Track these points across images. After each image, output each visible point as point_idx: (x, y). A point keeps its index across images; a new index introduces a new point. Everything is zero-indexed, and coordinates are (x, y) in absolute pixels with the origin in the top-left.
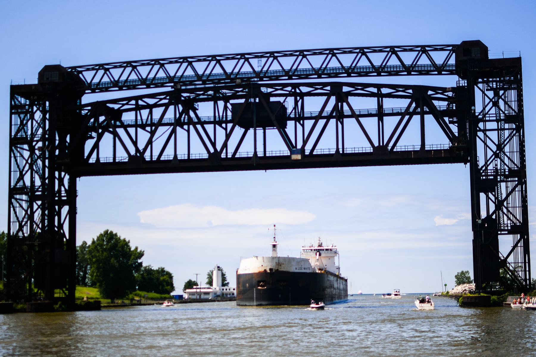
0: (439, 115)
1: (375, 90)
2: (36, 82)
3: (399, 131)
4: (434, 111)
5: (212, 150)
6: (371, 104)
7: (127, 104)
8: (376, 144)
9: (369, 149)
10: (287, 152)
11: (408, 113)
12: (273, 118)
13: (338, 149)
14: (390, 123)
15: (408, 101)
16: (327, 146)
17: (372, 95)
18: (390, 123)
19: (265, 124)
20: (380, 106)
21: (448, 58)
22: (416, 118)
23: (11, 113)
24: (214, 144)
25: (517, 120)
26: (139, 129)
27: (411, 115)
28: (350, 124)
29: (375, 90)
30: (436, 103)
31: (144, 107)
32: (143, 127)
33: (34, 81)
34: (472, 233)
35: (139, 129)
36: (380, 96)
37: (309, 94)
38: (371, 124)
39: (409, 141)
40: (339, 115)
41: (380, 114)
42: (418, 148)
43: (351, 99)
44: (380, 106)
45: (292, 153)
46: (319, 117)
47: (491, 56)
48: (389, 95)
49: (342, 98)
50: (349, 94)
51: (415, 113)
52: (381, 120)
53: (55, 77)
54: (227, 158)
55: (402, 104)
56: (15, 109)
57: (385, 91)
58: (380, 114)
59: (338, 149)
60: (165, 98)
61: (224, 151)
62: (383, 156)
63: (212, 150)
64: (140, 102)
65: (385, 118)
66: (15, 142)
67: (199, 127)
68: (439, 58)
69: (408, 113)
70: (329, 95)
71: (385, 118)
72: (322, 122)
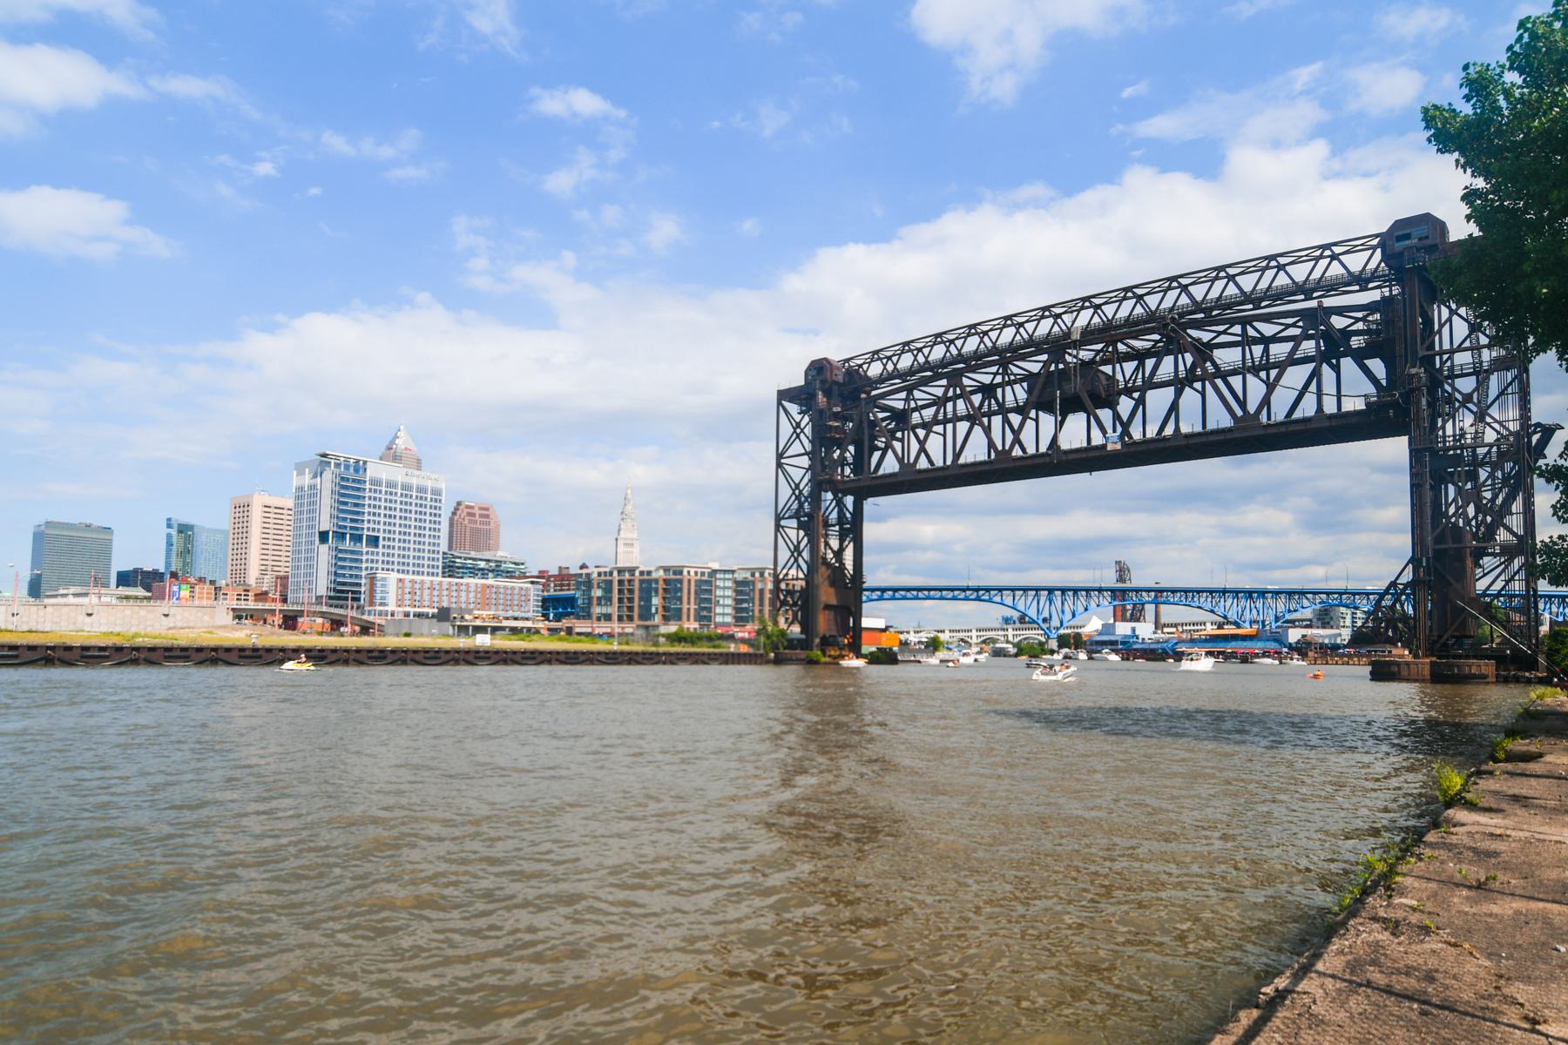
0: (1360, 357)
4: (1350, 352)
5: (1239, 413)
7: (1224, 332)
16: (976, 452)
24: (1243, 404)
26: (1249, 376)
31: (1255, 341)
32: (1255, 370)
35: (1249, 376)
54: (1145, 442)
60: (1294, 325)
61: (1265, 412)
63: (1239, 413)
64: (1121, 347)
67: (1219, 382)
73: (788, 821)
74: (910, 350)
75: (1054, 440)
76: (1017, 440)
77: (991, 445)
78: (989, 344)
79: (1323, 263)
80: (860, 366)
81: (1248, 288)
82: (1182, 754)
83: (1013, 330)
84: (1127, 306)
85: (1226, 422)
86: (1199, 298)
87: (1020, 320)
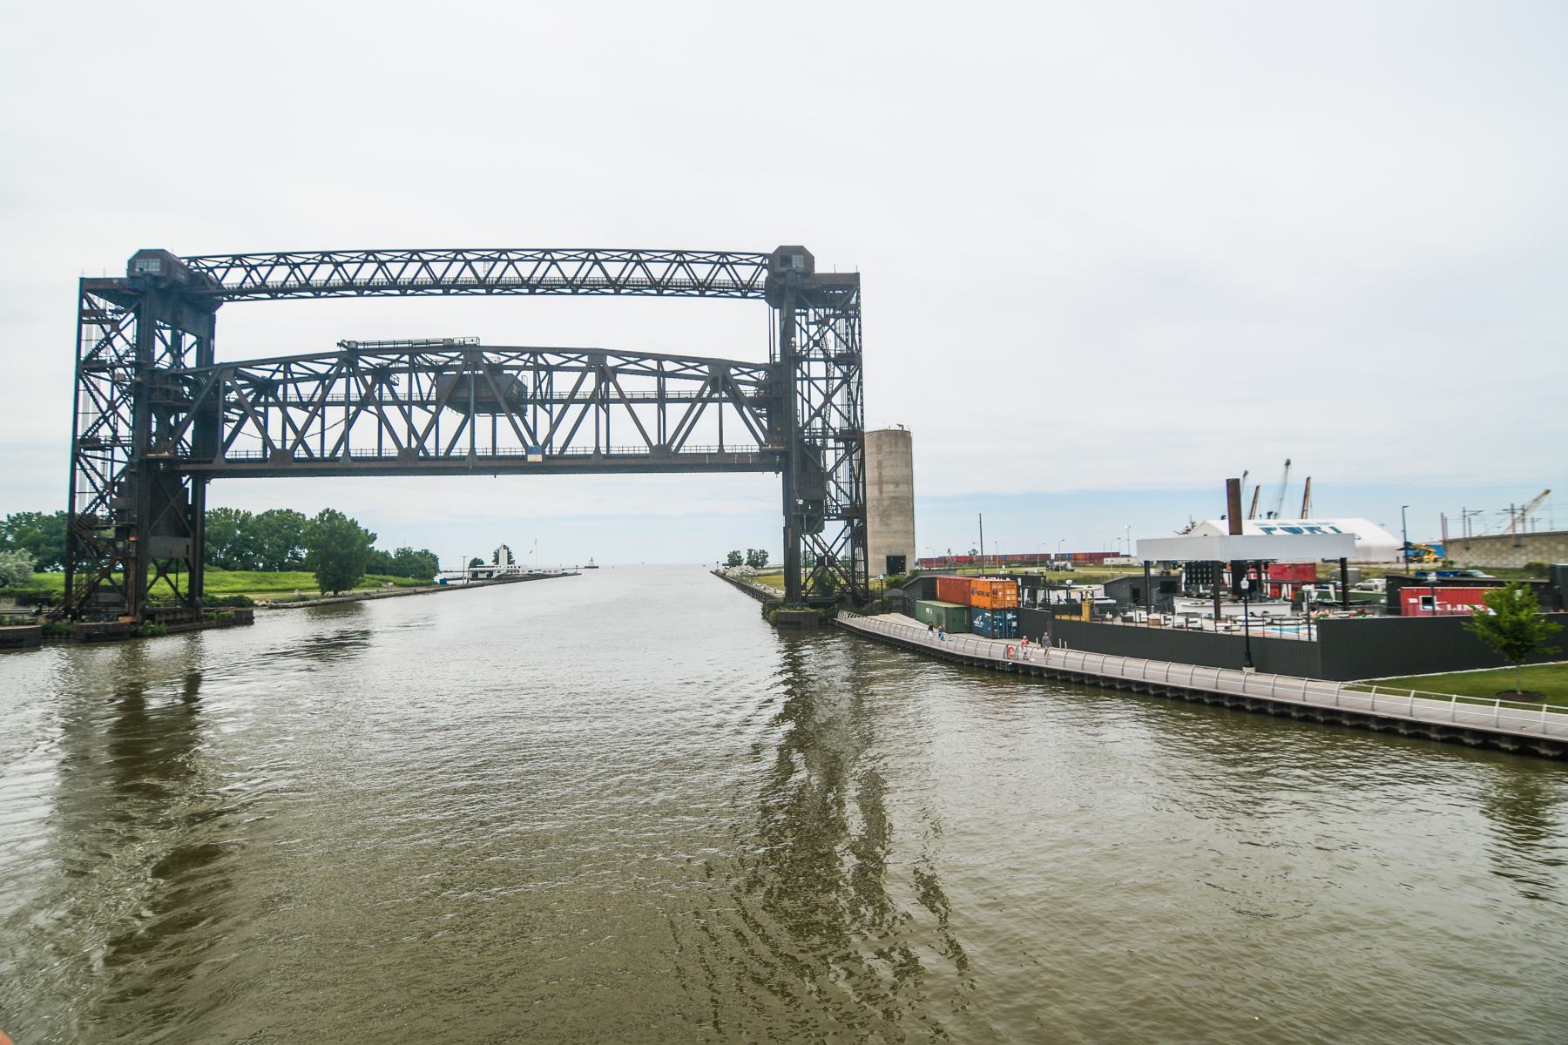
1: (653, 364)
2: (124, 275)
3: (687, 425)
5: (530, 443)
6: (649, 385)
8: (655, 442)
9: (644, 449)
10: (520, 451)
11: (700, 400)
12: (500, 399)
13: (597, 447)
14: (676, 412)
15: (702, 383)
16: (583, 443)
17: (651, 373)
18: (676, 412)
19: (493, 409)
20: (661, 390)
21: (756, 275)
22: (712, 408)
23: (81, 322)
24: (533, 435)
25: (850, 359)
27: (705, 402)
28: (618, 410)
29: (653, 364)
30: (742, 387)
33: (122, 273)
34: (783, 518)
36: (661, 374)
37: (558, 368)
38: (648, 413)
39: (702, 439)
40: (600, 400)
41: (662, 399)
42: (715, 450)
43: (620, 378)
44: (661, 390)
45: (529, 450)
46: (571, 400)
47: (820, 268)
48: (673, 374)
49: (606, 375)
50: (616, 370)
51: (710, 400)
52: (662, 408)
53: (154, 267)
55: (694, 387)
56: (88, 315)
57: (669, 366)
58: (662, 399)
59: (597, 447)
62: (664, 458)
63: (530, 443)
65: (668, 405)
66: (87, 367)
68: (745, 273)
69: (700, 400)
70: (584, 372)
71: (668, 405)
72: (575, 410)
73: (938, 904)
74: (242, 265)
75: (344, 438)
76: (300, 440)
77: (267, 442)
78: (258, 280)
79: (544, 265)
80: (211, 269)
81: (613, 274)
82: (569, 726)
83: (287, 269)
84: (413, 268)
85: (394, 452)
86: (526, 275)
87: (296, 260)
